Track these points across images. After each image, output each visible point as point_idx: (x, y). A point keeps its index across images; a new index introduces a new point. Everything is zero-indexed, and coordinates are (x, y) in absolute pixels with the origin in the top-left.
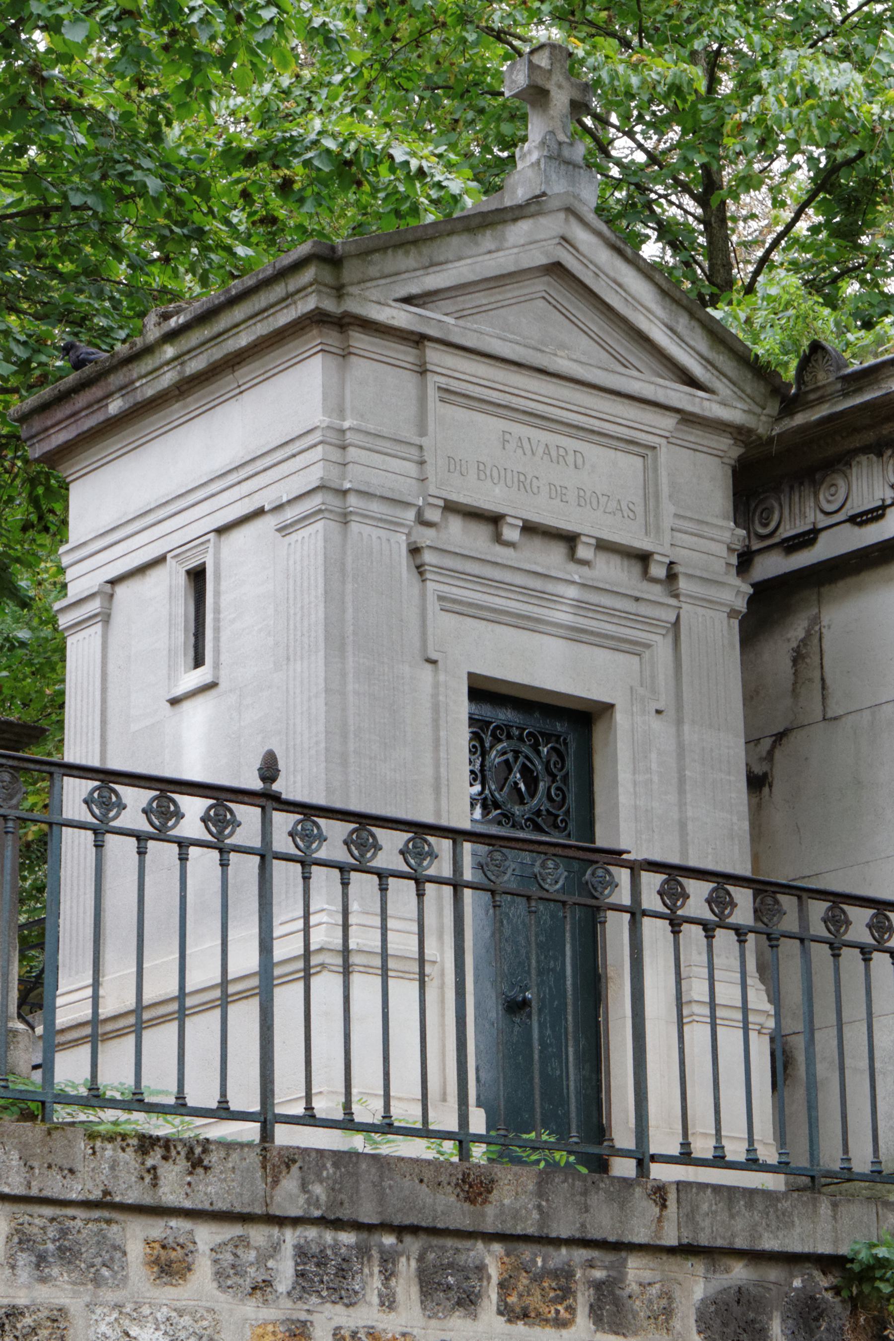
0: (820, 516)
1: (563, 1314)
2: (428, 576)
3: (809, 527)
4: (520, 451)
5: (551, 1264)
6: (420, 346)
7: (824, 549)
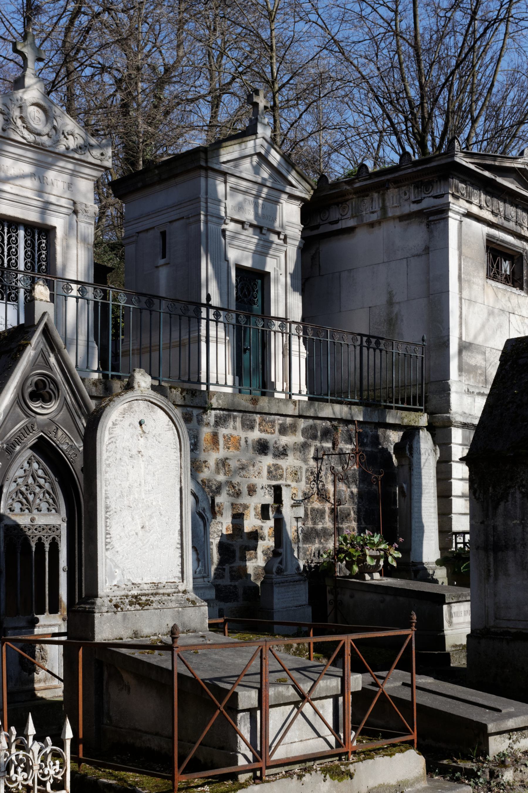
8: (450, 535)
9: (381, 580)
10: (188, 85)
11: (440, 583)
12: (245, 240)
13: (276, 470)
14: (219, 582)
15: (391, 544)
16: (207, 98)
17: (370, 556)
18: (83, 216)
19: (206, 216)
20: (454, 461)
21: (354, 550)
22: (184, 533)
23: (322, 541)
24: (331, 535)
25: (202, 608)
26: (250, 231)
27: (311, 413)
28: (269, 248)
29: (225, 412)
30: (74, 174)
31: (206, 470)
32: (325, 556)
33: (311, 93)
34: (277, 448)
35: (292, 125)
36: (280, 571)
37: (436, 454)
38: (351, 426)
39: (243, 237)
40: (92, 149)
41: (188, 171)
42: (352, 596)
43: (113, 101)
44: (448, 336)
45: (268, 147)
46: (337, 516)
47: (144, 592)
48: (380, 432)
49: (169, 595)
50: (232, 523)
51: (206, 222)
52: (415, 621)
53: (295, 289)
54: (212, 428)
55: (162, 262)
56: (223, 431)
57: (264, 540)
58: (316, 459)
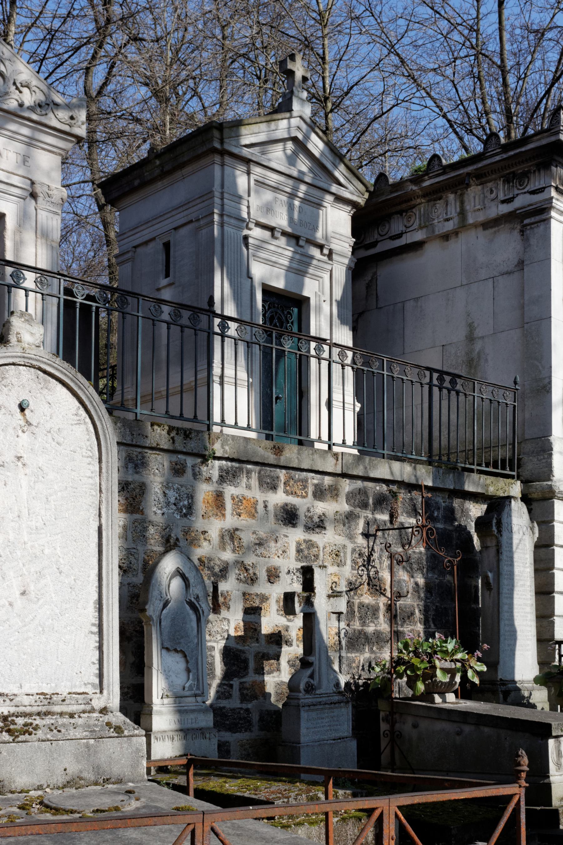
1: (304, 494)
5: (301, 477)
7: (380, 248)
8: (550, 646)
9: (456, 703)
11: (539, 708)
12: (274, 252)
13: (309, 548)
14: (224, 703)
15: (471, 652)
17: (442, 669)
18: (44, 202)
19: (221, 215)
20: (557, 546)
21: (419, 660)
22: (104, 607)
23: (374, 648)
24: (388, 642)
25: (134, 739)
26: (283, 241)
27: (359, 471)
28: (309, 264)
29: (234, 464)
30: (31, 142)
31: (205, 544)
32: (378, 669)
34: (311, 518)
36: (310, 689)
37: (533, 533)
38: (416, 494)
39: (272, 248)
40: (57, 109)
41: (198, 158)
42: (415, 726)
44: (550, 377)
45: (307, 131)
46: (395, 616)
47: (21, 709)
48: (456, 503)
49: (72, 716)
50: (243, 621)
51: (222, 225)
52: (526, 768)
53: (343, 321)
54: (215, 485)
55: (164, 282)
56: (230, 491)
57: (291, 645)
58: (366, 535)
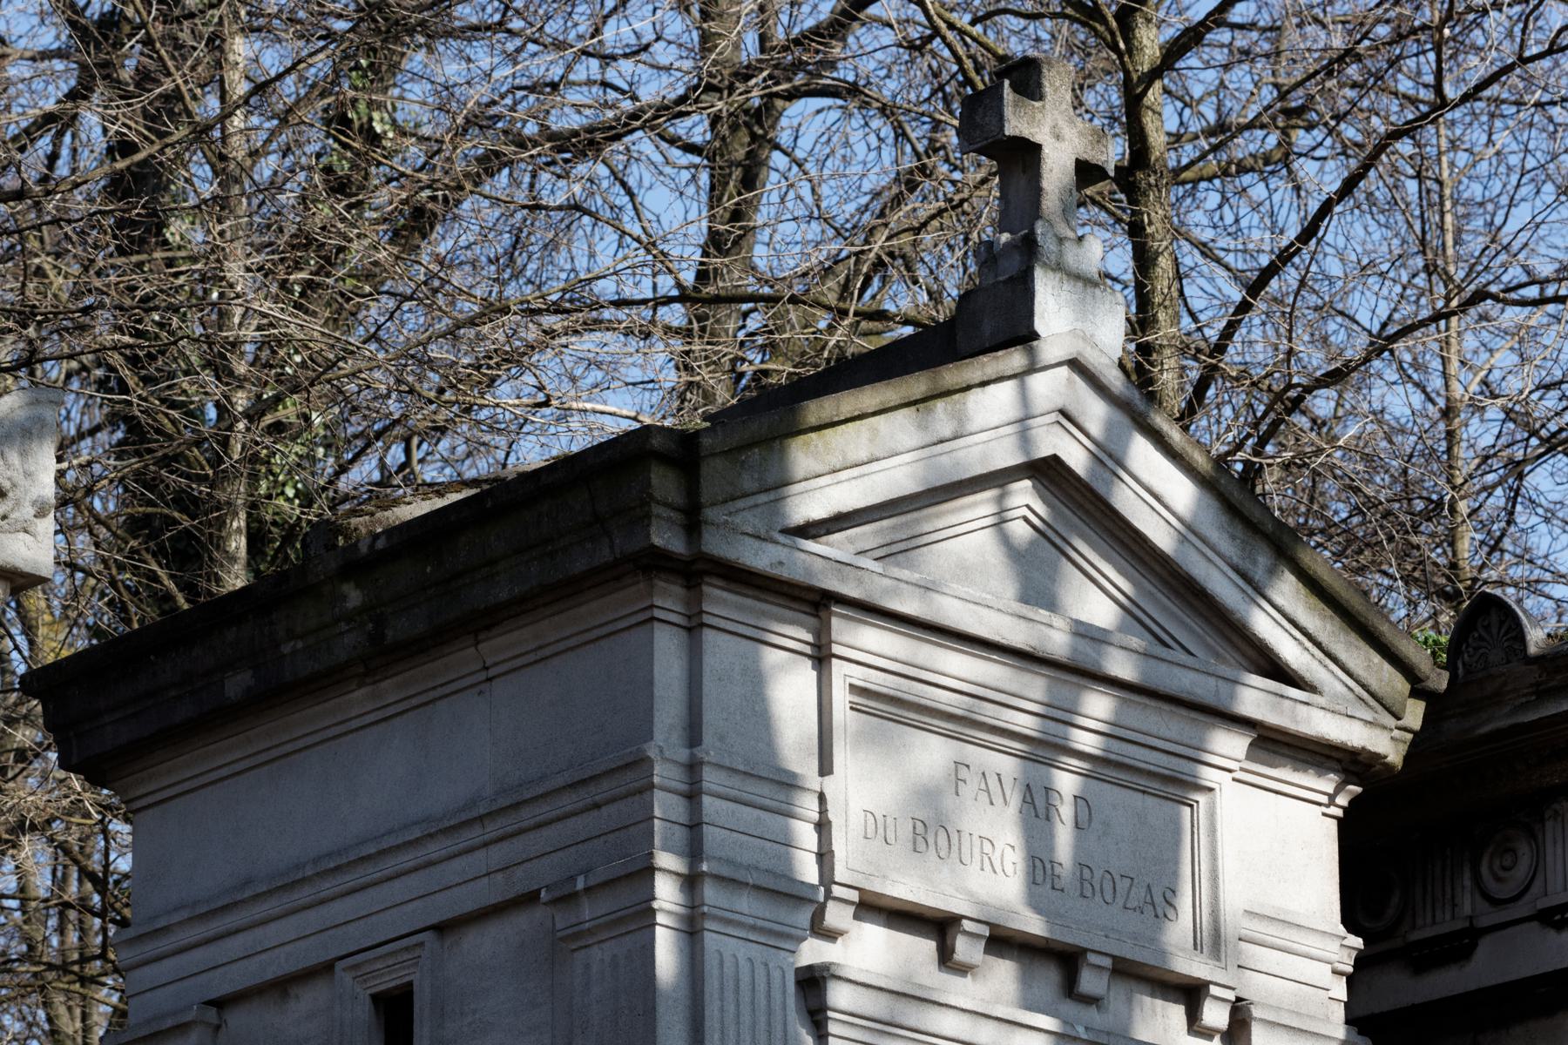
0: (1482, 905)
2: (833, 1028)
3: (1460, 925)
4: (983, 797)
6: (823, 614)
10: (560, 45)
16: (681, 128)
19: (691, 882)
33: (1376, 81)
35: (1255, 288)
43: (53, 158)
45: (1109, 427)
51: (692, 928)
